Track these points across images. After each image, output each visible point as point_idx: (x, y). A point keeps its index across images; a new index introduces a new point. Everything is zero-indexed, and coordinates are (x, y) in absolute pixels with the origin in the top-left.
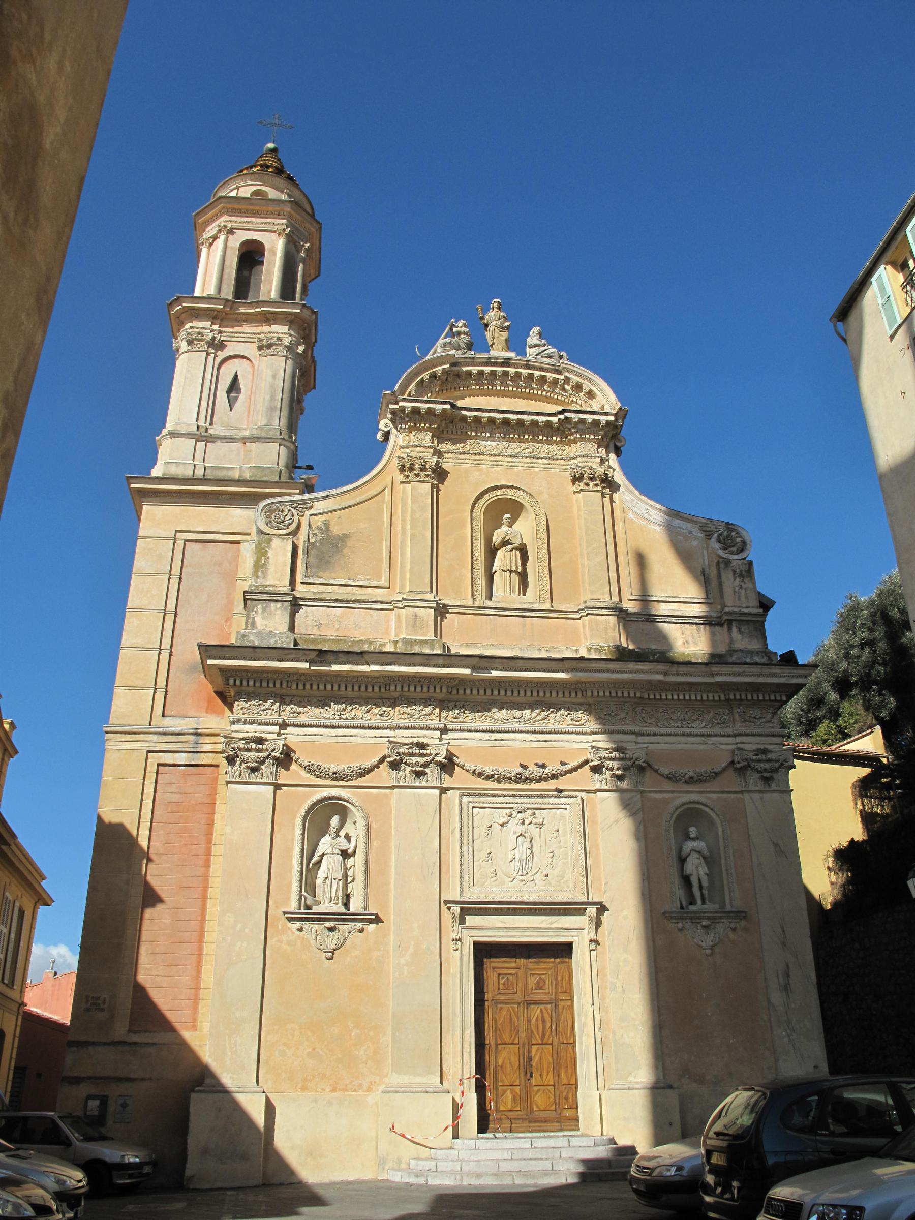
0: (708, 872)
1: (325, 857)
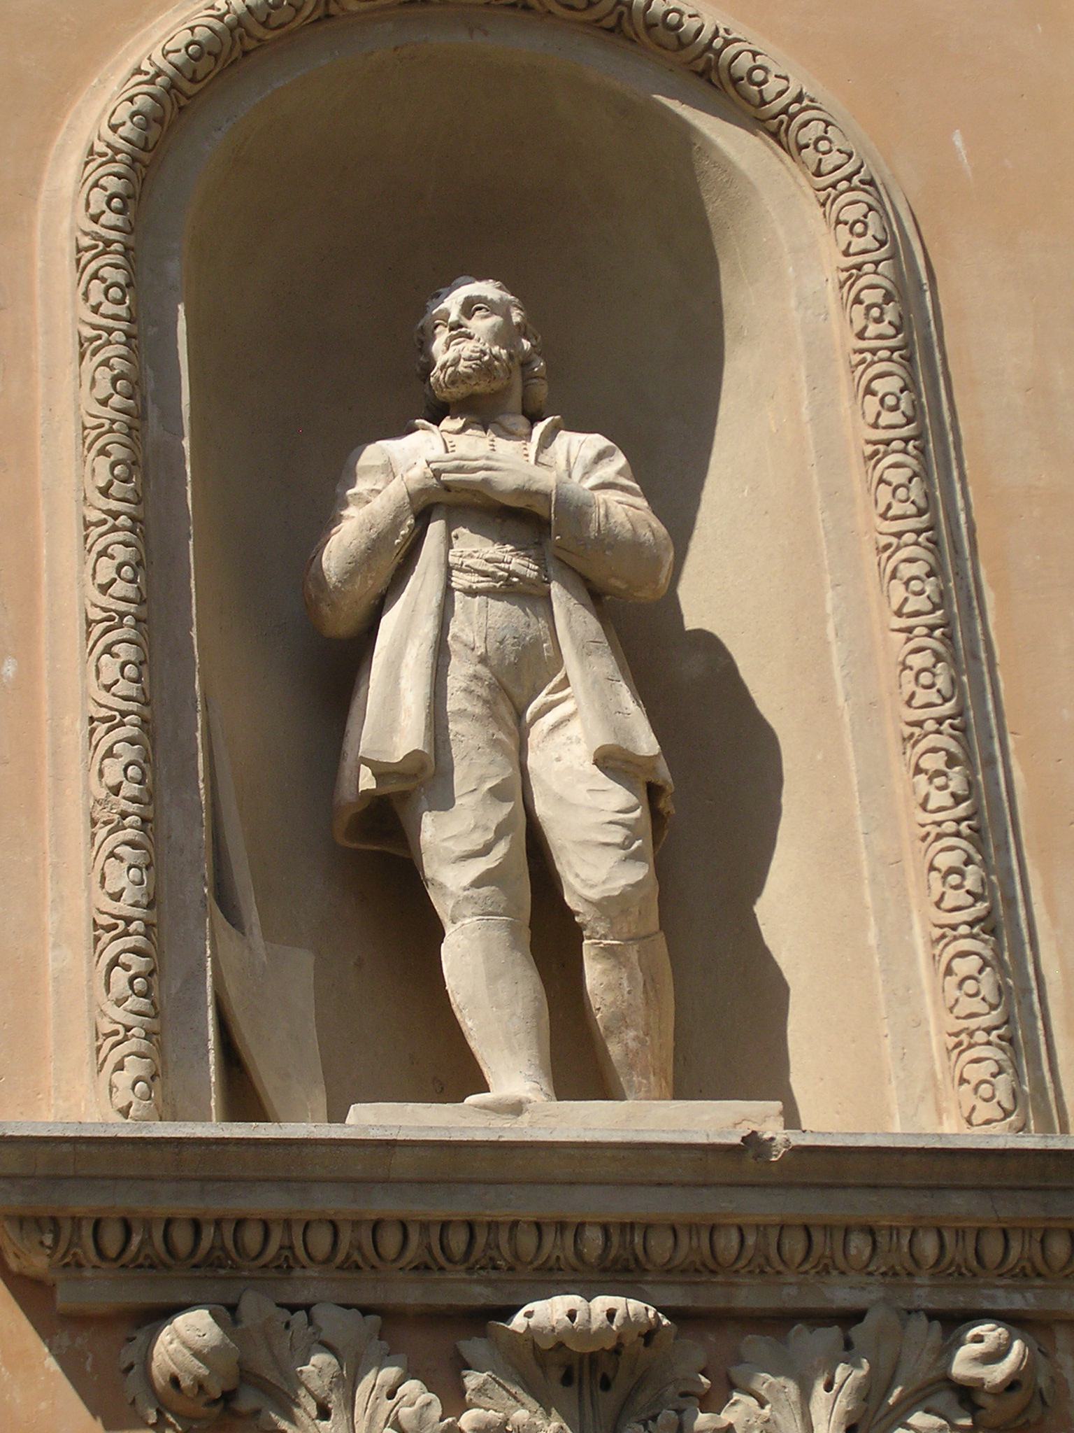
0: (646, 743)
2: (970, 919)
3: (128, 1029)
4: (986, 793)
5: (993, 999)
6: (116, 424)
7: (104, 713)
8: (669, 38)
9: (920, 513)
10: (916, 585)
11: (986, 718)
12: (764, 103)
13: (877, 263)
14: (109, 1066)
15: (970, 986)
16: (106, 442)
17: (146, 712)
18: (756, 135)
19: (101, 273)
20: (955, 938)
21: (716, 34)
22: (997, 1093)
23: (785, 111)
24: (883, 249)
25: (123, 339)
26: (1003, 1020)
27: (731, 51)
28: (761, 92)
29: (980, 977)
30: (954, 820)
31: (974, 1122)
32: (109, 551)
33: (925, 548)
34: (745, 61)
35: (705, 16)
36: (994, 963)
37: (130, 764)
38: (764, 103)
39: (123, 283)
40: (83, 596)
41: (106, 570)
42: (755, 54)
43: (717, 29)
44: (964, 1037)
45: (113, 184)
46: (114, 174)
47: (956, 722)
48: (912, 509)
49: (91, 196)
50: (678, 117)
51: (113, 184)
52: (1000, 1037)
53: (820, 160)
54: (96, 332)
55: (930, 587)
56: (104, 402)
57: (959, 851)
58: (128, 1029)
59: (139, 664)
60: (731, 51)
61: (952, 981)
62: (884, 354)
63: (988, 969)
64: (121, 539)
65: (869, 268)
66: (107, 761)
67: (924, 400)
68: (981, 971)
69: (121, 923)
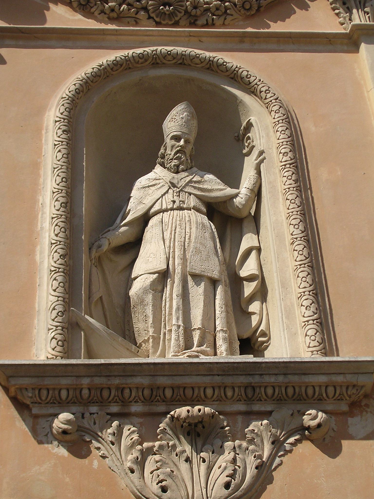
1: (153, 222)
2: (317, 350)
3: (62, 190)
4: (307, 211)
5: (299, 204)
6: (60, 269)
7: (55, 216)
8: (224, 69)
9: (289, 137)
10: (304, 279)
11: (309, 202)
12: (250, 83)
13: (283, 120)
14: (56, 175)
15: (296, 227)
16: (54, 305)
17: (70, 119)
18: (250, 95)
19: (58, 224)
20: (308, 325)
21: (237, 67)
22: (317, 339)
23: (256, 84)
24: (321, 346)
25: (64, 244)
26: (318, 317)
27: (241, 70)
28: (249, 81)
29: (299, 224)
30: (308, 291)
31: (300, 287)
32: (58, 224)
33: (303, 241)
34: (245, 73)
35: (233, 62)
36: (299, 196)
37: (60, 312)
38: (250, 83)
39: (63, 311)
40: (47, 323)
41: (55, 284)
42: (248, 71)
43: (237, 66)
44: (291, 213)
45: (63, 175)
46: (62, 222)
47: (305, 238)
48: (287, 137)
49: (52, 294)
50: (227, 90)
51: (63, 175)
52: (313, 293)
53: (266, 95)
54: (55, 269)
55: (287, 132)
56: (58, 210)
57: (302, 245)
58: (62, 190)
59: (68, 154)
60: (241, 70)
61: (299, 279)
62: (288, 166)
63: (318, 333)
64: (61, 247)
65: (281, 121)
66: (58, 130)
67: (325, 337)
68: (307, 276)
69: (58, 242)
